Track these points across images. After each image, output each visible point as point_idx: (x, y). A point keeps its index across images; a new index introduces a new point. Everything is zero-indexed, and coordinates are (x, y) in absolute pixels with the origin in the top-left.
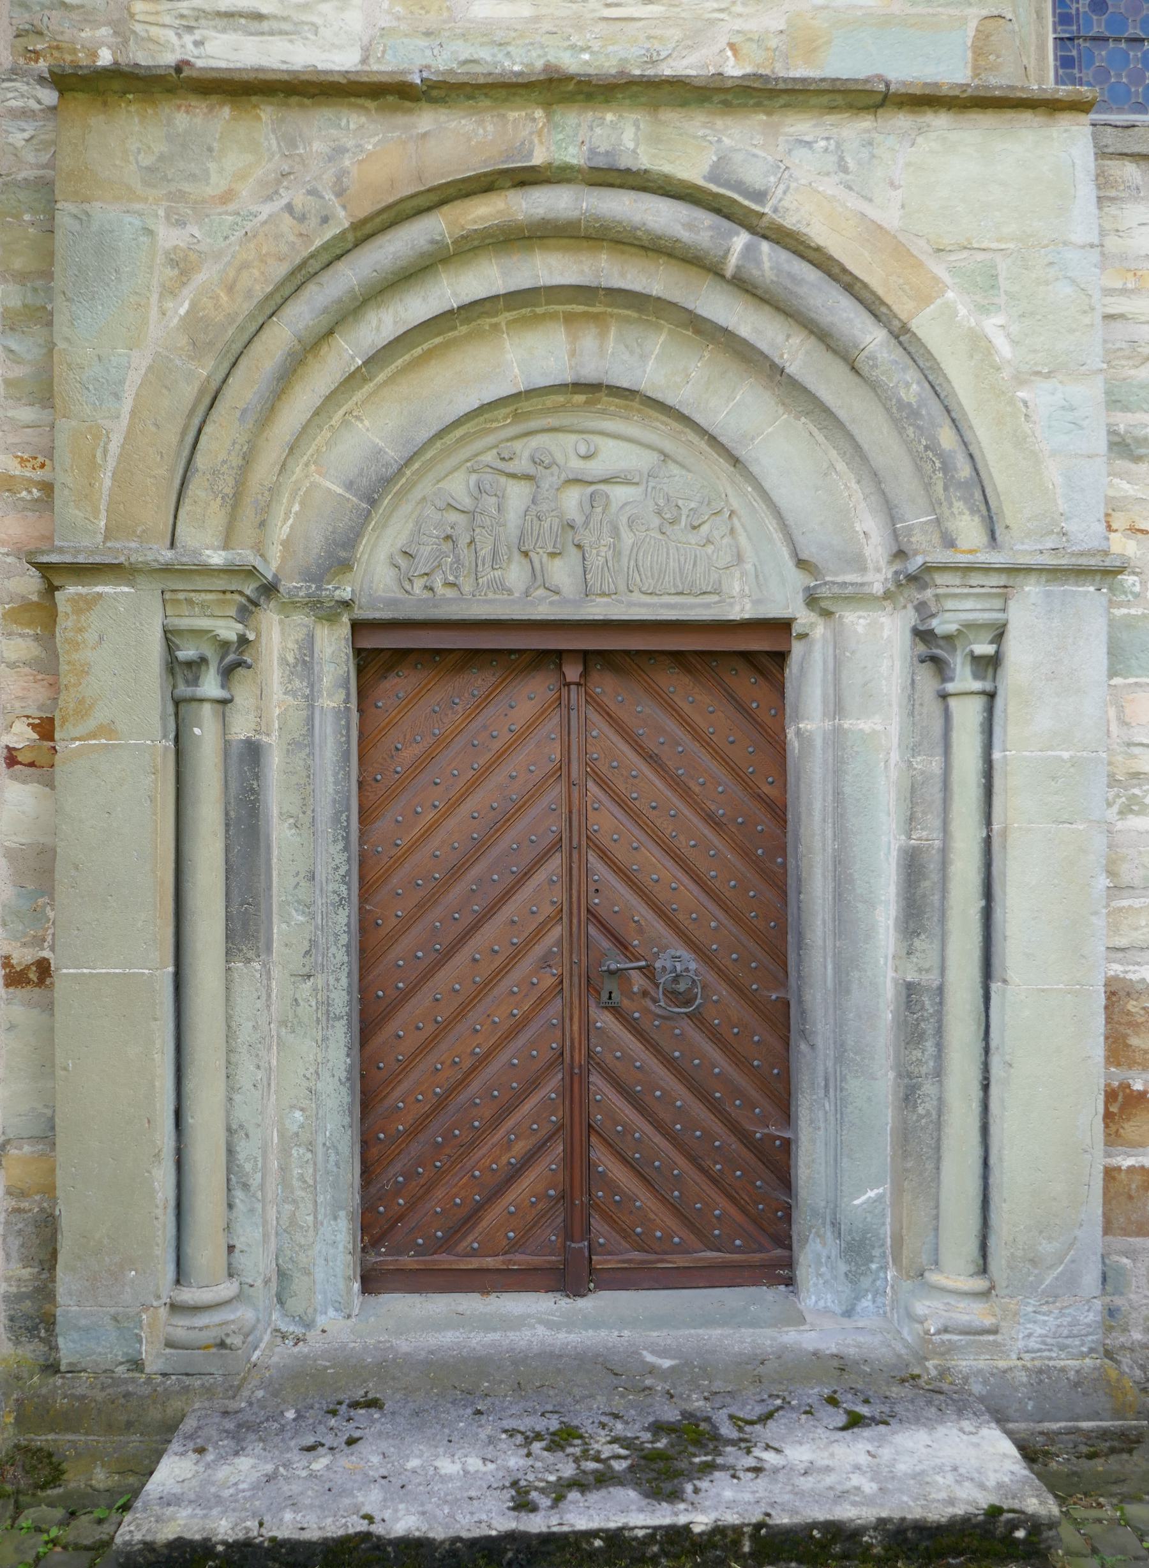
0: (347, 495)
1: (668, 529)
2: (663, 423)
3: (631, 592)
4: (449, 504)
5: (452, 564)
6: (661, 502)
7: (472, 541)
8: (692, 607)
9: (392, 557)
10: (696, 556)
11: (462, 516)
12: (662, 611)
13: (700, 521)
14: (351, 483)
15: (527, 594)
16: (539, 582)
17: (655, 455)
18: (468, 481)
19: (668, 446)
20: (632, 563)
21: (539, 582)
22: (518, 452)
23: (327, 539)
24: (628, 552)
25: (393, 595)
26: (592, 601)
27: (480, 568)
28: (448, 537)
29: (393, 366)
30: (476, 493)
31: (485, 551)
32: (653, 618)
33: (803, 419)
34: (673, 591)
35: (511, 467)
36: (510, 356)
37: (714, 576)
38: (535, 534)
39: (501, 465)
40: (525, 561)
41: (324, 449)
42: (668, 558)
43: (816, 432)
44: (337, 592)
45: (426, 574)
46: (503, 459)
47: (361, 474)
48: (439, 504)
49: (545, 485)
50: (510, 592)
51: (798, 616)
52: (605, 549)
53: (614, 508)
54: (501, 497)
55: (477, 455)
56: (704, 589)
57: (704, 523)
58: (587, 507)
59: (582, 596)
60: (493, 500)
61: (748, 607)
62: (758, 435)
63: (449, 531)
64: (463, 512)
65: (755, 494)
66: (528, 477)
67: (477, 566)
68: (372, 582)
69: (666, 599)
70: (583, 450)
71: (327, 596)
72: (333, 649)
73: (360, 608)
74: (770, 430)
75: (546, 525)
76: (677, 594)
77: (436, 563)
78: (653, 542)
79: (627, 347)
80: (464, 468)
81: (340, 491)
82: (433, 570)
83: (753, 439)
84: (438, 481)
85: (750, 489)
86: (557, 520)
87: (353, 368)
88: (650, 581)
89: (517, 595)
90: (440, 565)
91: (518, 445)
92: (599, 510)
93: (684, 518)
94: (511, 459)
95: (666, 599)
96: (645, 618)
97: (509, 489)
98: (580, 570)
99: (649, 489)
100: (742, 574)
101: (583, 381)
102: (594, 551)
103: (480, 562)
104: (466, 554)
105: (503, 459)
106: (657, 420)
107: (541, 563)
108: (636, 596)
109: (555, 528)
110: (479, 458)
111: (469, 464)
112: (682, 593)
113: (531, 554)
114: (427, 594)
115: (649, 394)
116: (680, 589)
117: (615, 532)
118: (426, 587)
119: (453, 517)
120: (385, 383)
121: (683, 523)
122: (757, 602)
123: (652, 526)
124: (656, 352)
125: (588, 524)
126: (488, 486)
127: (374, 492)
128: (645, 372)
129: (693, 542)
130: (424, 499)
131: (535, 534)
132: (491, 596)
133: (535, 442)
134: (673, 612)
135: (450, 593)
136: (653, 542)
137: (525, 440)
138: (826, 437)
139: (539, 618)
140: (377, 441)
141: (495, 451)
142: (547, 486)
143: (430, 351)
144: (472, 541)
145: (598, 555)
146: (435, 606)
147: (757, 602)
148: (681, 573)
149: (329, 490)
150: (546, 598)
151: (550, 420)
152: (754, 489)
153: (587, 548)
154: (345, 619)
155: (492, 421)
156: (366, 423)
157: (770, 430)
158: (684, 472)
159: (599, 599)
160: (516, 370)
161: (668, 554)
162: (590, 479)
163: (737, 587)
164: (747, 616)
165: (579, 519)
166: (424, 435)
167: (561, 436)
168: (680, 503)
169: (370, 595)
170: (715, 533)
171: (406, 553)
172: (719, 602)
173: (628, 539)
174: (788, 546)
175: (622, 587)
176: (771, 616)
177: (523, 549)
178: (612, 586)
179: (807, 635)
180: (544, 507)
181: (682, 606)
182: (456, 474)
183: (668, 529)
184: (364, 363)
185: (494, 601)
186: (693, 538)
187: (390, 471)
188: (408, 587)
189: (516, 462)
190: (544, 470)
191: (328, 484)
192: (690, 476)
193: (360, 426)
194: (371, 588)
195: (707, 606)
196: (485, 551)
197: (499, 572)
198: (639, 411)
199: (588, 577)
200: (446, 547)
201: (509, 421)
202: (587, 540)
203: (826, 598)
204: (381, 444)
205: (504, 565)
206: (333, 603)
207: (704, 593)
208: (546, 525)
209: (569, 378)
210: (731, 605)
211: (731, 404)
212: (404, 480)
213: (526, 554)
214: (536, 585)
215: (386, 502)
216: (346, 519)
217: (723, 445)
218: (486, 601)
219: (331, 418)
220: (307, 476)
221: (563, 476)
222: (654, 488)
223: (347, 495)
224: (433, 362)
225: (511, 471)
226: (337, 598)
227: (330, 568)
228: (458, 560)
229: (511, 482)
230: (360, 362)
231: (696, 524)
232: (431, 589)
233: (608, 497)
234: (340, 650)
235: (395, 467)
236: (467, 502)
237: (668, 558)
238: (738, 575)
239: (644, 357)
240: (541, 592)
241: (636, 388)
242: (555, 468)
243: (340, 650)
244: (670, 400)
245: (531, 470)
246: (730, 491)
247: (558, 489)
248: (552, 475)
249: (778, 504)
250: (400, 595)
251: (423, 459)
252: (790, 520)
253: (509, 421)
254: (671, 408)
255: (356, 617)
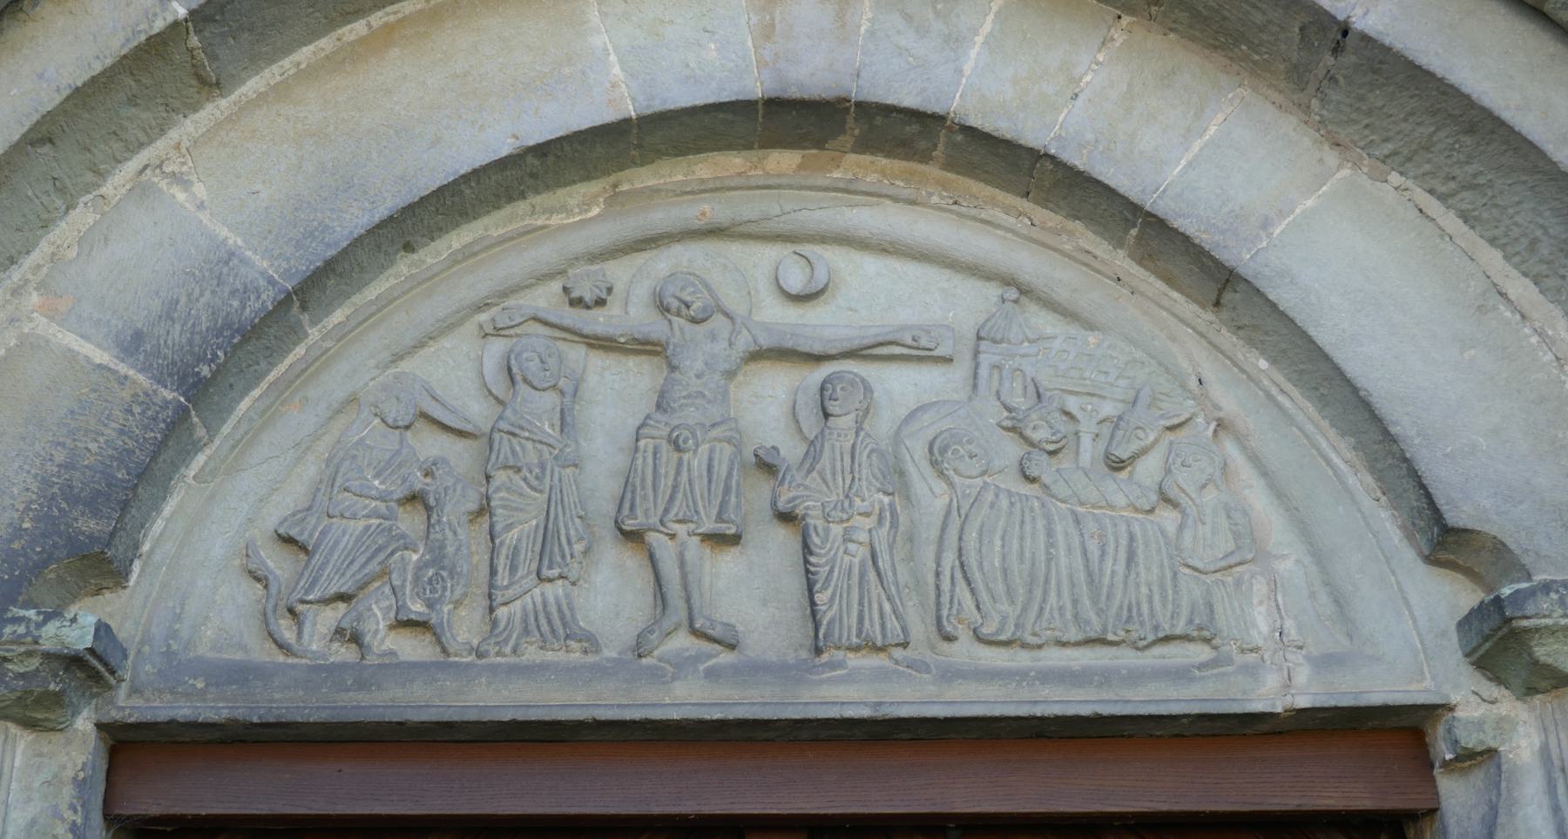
0: (123, 368)
1: (1041, 466)
2: (1007, 210)
3: (949, 638)
4: (424, 416)
5: (421, 567)
6: (1018, 401)
7: (484, 509)
8: (1136, 677)
9: (248, 551)
10: (1132, 538)
11: (460, 445)
12: (1046, 692)
13: (1134, 447)
14: (138, 337)
15: (640, 649)
16: (678, 611)
17: (992, 291)
18: (480, 360)
19: (1028, 263)
20: (949, 559)
21: (678, 611)
22: (619, 288)
23: (46, 482)
24: (934, 533)
25: (239, 656)
26: (833, 666)
27: (502, 578)
28: (414, 498)
29: (286, 62)
30: (500, 388)
31: (520, 530)
32: (1023, 711)
33: (1395, 178)
34: (1073, 634)
35: (597, 322)
36: (599, 40)
37: (1191, 589)
38: (665, 484)
39: (573, 317)
40: (632, 560)
41: (72, 254)
42: (1050, 544)
43: (1434, 206)
44: (51, 628)
45: (343, 597)
46: (577, 302)
47: (168, 315)
48: (394, 411)
49: (692, 362)
50: (590, 642)
51: (1454, 698)
52: (869, 523)
53: (883, 424)
54: (570, 395)
55: (506, 294)
56: (1166, 629)
57: (1144, 451)
58: (811, 424)
59: (804, 654)
60: (549, 400)
61: (1302, 676)
62: (1282, 215)
63: (418, 481)
64: (461, 434)
65: (1280, 378)
66: (645, 347)
67: (493, 572)
68: (178, 618)
69: (1055, 658)
70: (795, 280)
71: (18, 640)
72: (32, 810)
73: (135, 690)
74: (1310, 203)
75: (697, 462)
76: (1088, 642)
77: (374, 566)
78: (1004, 503)
79: (908, 18)
80: (470, 327)
81: (101, 357)
82: (363, 586)
83: (1266, 224)
84: (398, 358)
85: (1263, 364)
86: (728, 450)
87: (159, 25)
88: (1005, 607)
89: (610, 653)
90: (385, 573)
91: (619, 272)
92: (844, 422)
93: (1086, 441)
94: (600, 302)
95: (1055, 658)
96: (997, 711)
97: (592, 379)
98: (793, 585)
99: (983, 372)
100: (1274, 585)
101: (794, 93)
102: (837, 530)
103: (502, 562)
104: (468, 544)
105: (577, 302)
106: (993, 202)
107: (682, 564)
108: (965, 651)
109: (721, 469)
110: (511, 302)
111: (483, 317)
112: (1102, 641)
113: (652, 537)
114: (344, 653)
115: (974, 121)
116: (1094, 630)
117: (896, 479)
118: (339, 632)
119: (431, 445)
120: (262, 98)
121: (1086, 457)
122: (1325, 663)
123: (998, 463)
124: (987, 27)
125: (816, 460)
126: (534, 366)
127: (200, 359)
128: (959, 72)
129: (1120, 500)
130: (352, 400)
131: (665, 484)
132: (532, 654)
133: (663, 262)
134: (1078, 694)
135: (412, 648)
136: (1004, 503)
137: (639, 259)
138: (1465, 217)
139: (675, 714)
140: (224, 232)
141: (556, 286)
142: (699, 365)
143: (389, 29)
144: (484, 509)
145: (847, 539)
146: (361, 685)
147: (1325, 663)
148: (1091, 579)
149: (71, 356)
150: (699, 658)
151: (706, 207)
152: (1273, 361)
153: (816, 521)
154: (84, 723)
155: (551, 211)
156: (199, 190)
157: (1310, 203)
158: (1073, 330)
159: (854, 660)
160: (617, 70)
161: (1050, 533)
162: (817, 348)
163: (1261, 623)
164: (1303, 702)
165: (790, 450)
166: (357, 218)
167: (735, 251)
168: (1072, 404)
169: (169, 654)
170: (1182, 476)
171: (288, 540)
172: (1214, 663)
173: (932, 497)
174: (1396, 502)
175: (920, 629)
176: (1376, 699)
177: (629, 525)
178: (893, 624)
179: (1491, 753)
180: (691, 415)
181: (1106, 677)
182: (446, 342)
183: (1041, 466)
184: (192, 13)
185: (543, 667)
186: (1117, 490)
187: (253, 305)
188: (289, 635)
189: (614, 309)
190: (688, 326)
191: (71, 340)
192: (1092, 338)
193: (181, 196)
194: (174, 634)
195: (1181, 674)
196: (520, 530)
197: (559, 588)
198: (944, 185)
199: (820, 598)
200: (410, 522)
201: (595, 211)
202: (811, 500)
203: (1552, 631)
204: (235, 240)
205: (574, 571)
206: (35, 663)
207: (1168, 639)
208: (697, 462)
209: (754, 87)
210: (1252, 671)
211: (1197, 146)
212: (300, 350)
213: (633, 537)
214: (667, 624)
215: (244, 405)
216: (110, 432)
217: (1186, 239)
218: (513, 670)
219: (102, 175)
220: (12, 321)
221: (743, 343)
222: (997, 367)
223: (123, 368)
224: (395, 52)
225: (600, 330)
226: (47, 645)
227: (45, 564)
228: (437, 557)
229: (597, 360)
230: (182, 12)
231: (1123, 452)
232: (356, 639)
233: (868, 389)
234: (57, 815)
235: (268, 298)
236: (477, 412)
237: (1050, 544)
238: (1260, 587)
239: (955, 42)
240: (682, 642)
241: (937, 109)
242: (718, 321)
243: (57, 815)
244: (1033, 133)
245: (655, 327)
246: (1208, 374)
247: (730, 374)
248: (713, 337)
249: (1361, 382)
250: (262, 653)
251: (358, 299)
252: (1402, 423)
253: (595, 211)
254: (1037, 156)
255: (114, 715)
